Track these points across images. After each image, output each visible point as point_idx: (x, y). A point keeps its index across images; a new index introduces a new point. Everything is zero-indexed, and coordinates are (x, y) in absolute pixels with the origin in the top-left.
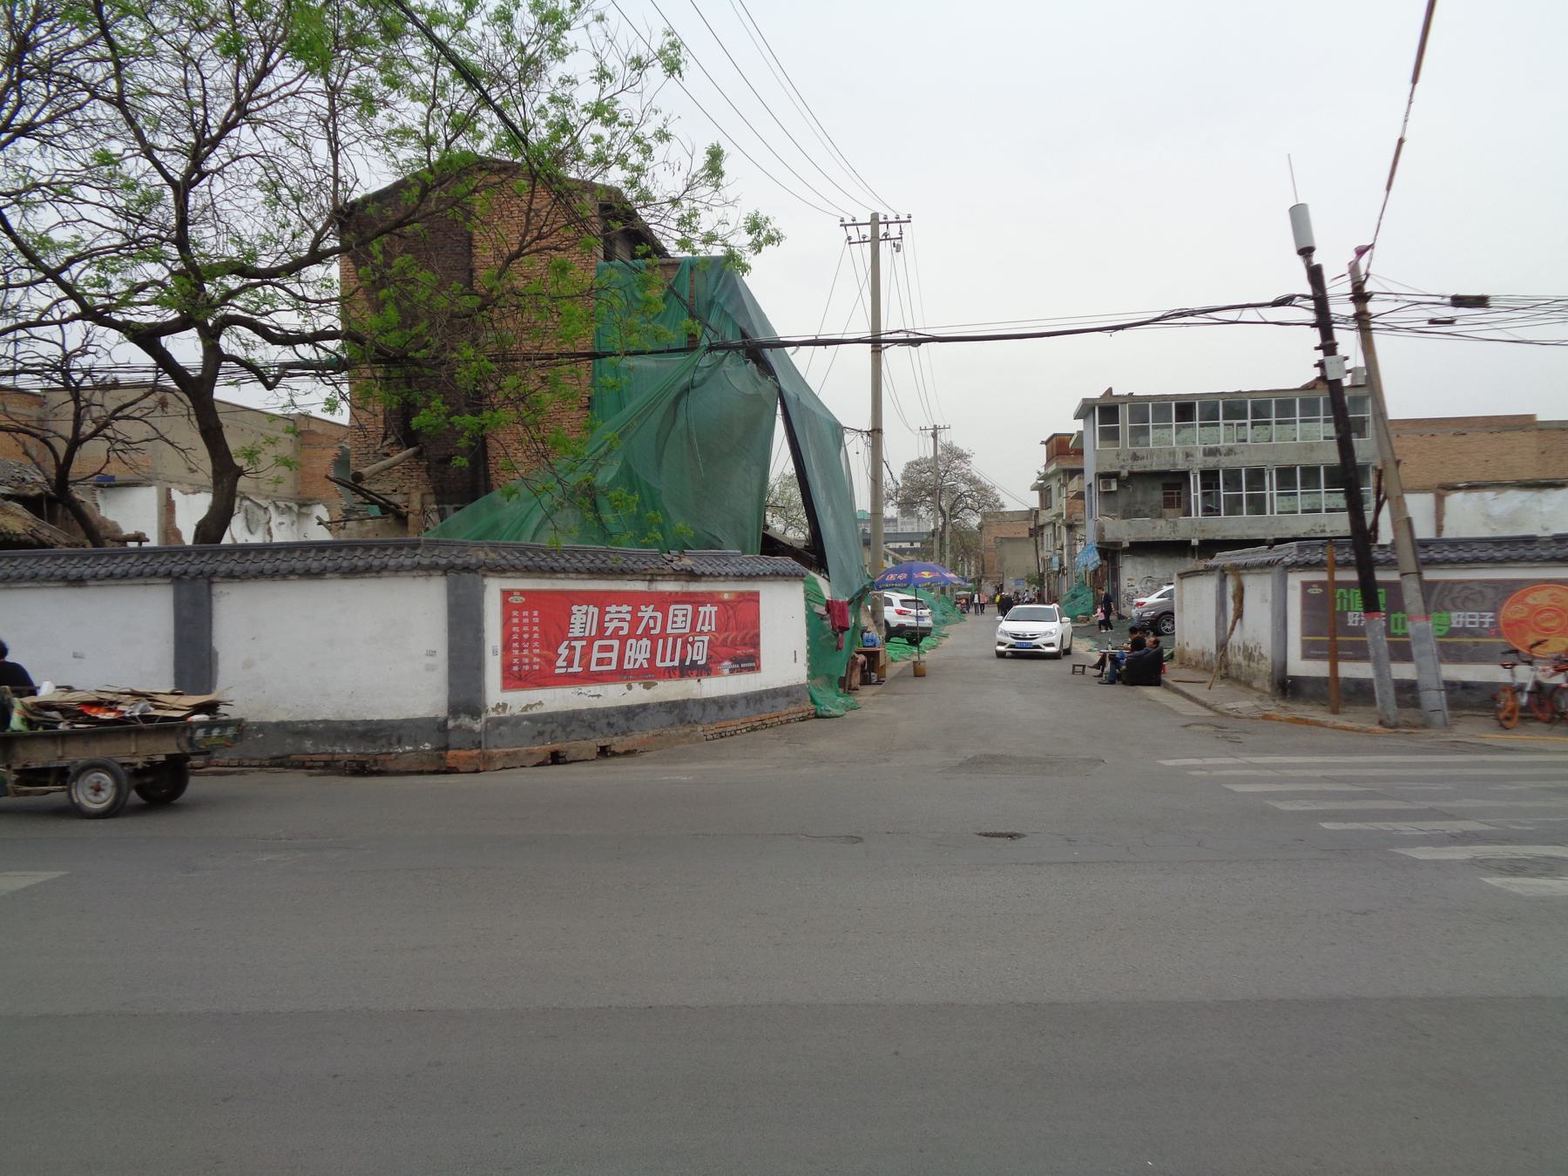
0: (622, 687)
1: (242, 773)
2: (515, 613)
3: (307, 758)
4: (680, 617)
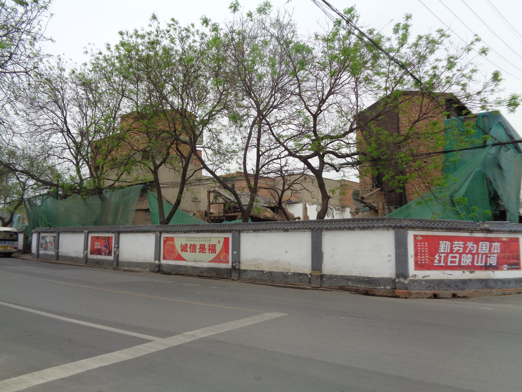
0: (460, 272)
1: (330, 291)
2: (419, 243)
3: (350, 288)
4: (484, 247)
